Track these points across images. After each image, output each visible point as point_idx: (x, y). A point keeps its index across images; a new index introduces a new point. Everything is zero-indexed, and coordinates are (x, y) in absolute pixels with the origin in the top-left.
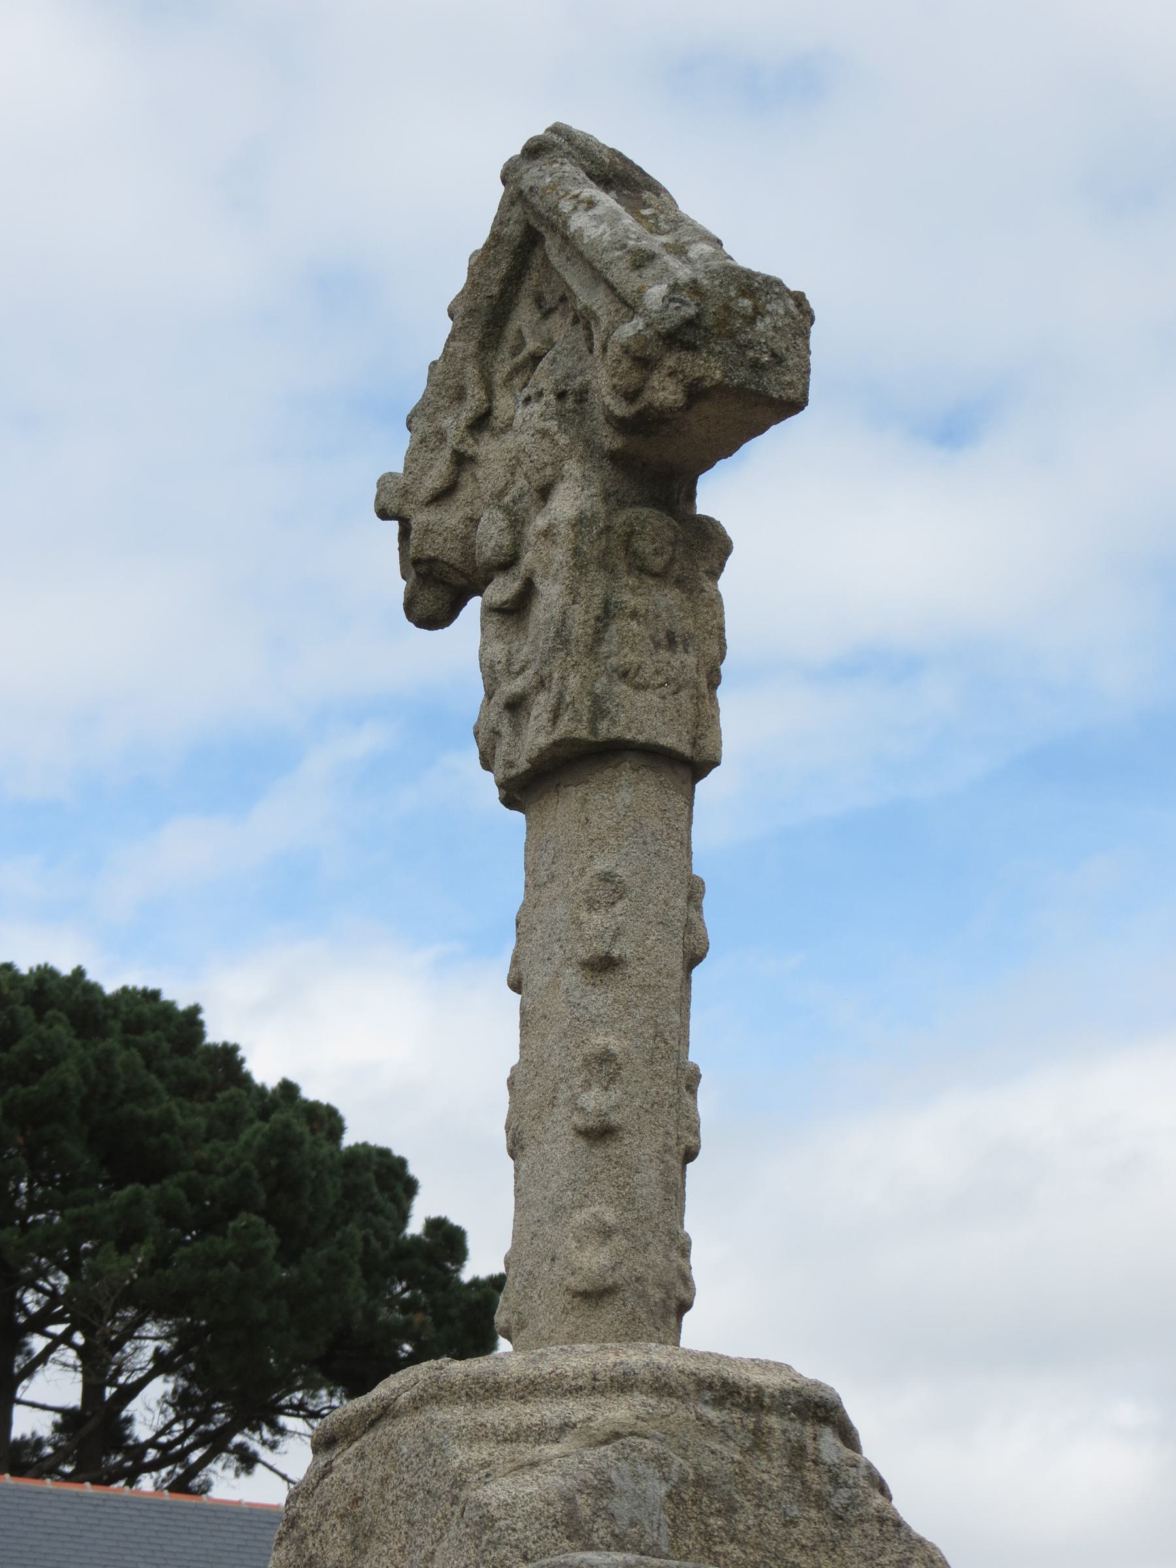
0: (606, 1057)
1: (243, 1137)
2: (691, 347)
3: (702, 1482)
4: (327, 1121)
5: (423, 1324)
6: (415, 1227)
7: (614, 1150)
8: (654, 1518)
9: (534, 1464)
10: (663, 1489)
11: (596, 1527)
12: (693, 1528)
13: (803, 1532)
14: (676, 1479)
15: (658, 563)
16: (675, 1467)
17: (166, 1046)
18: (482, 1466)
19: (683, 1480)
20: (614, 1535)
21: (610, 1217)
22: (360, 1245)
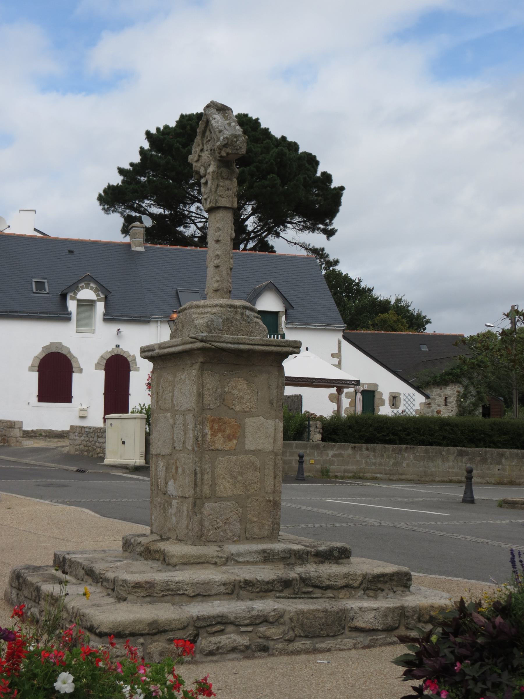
0: (218, 255)
1: (271, 153)
2: (227, 148)
3: (227, 319)
4: (294, 146)
5: (321, 200)
6: (319, 174)
7: (219, 269)
13: (243, 325)
15: (226, 177)
17: (250, 129)
21: (218, 279)
22: (302, 180)
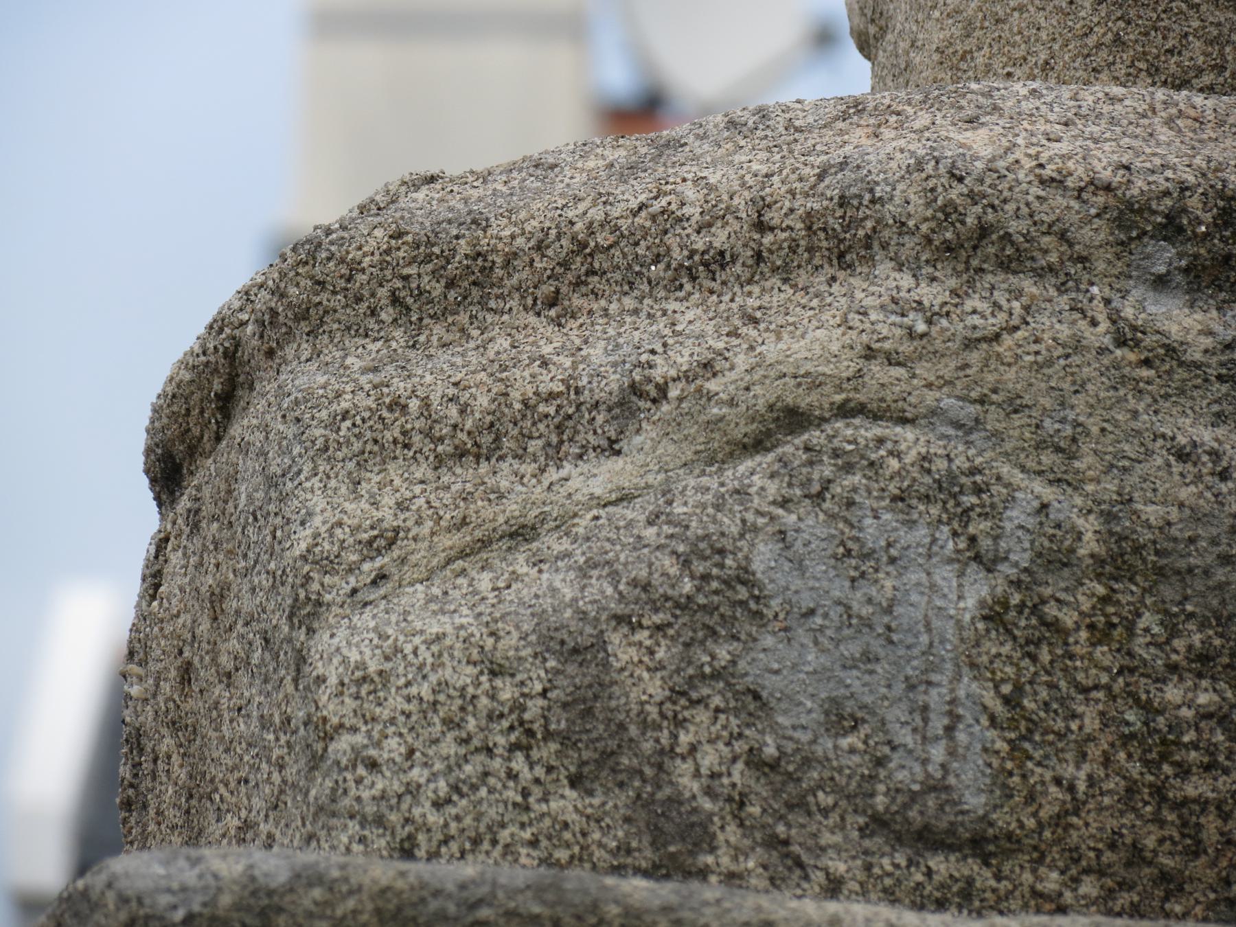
8: (935, 698)
9: (521, 533)
10: (977, 590)
11: (685, 738)
12: (1091, 723)
14: (1024, 559)
16: (1017, 516)
18: (371, 548)
19: (1056, 558)
20: (754, 760)
